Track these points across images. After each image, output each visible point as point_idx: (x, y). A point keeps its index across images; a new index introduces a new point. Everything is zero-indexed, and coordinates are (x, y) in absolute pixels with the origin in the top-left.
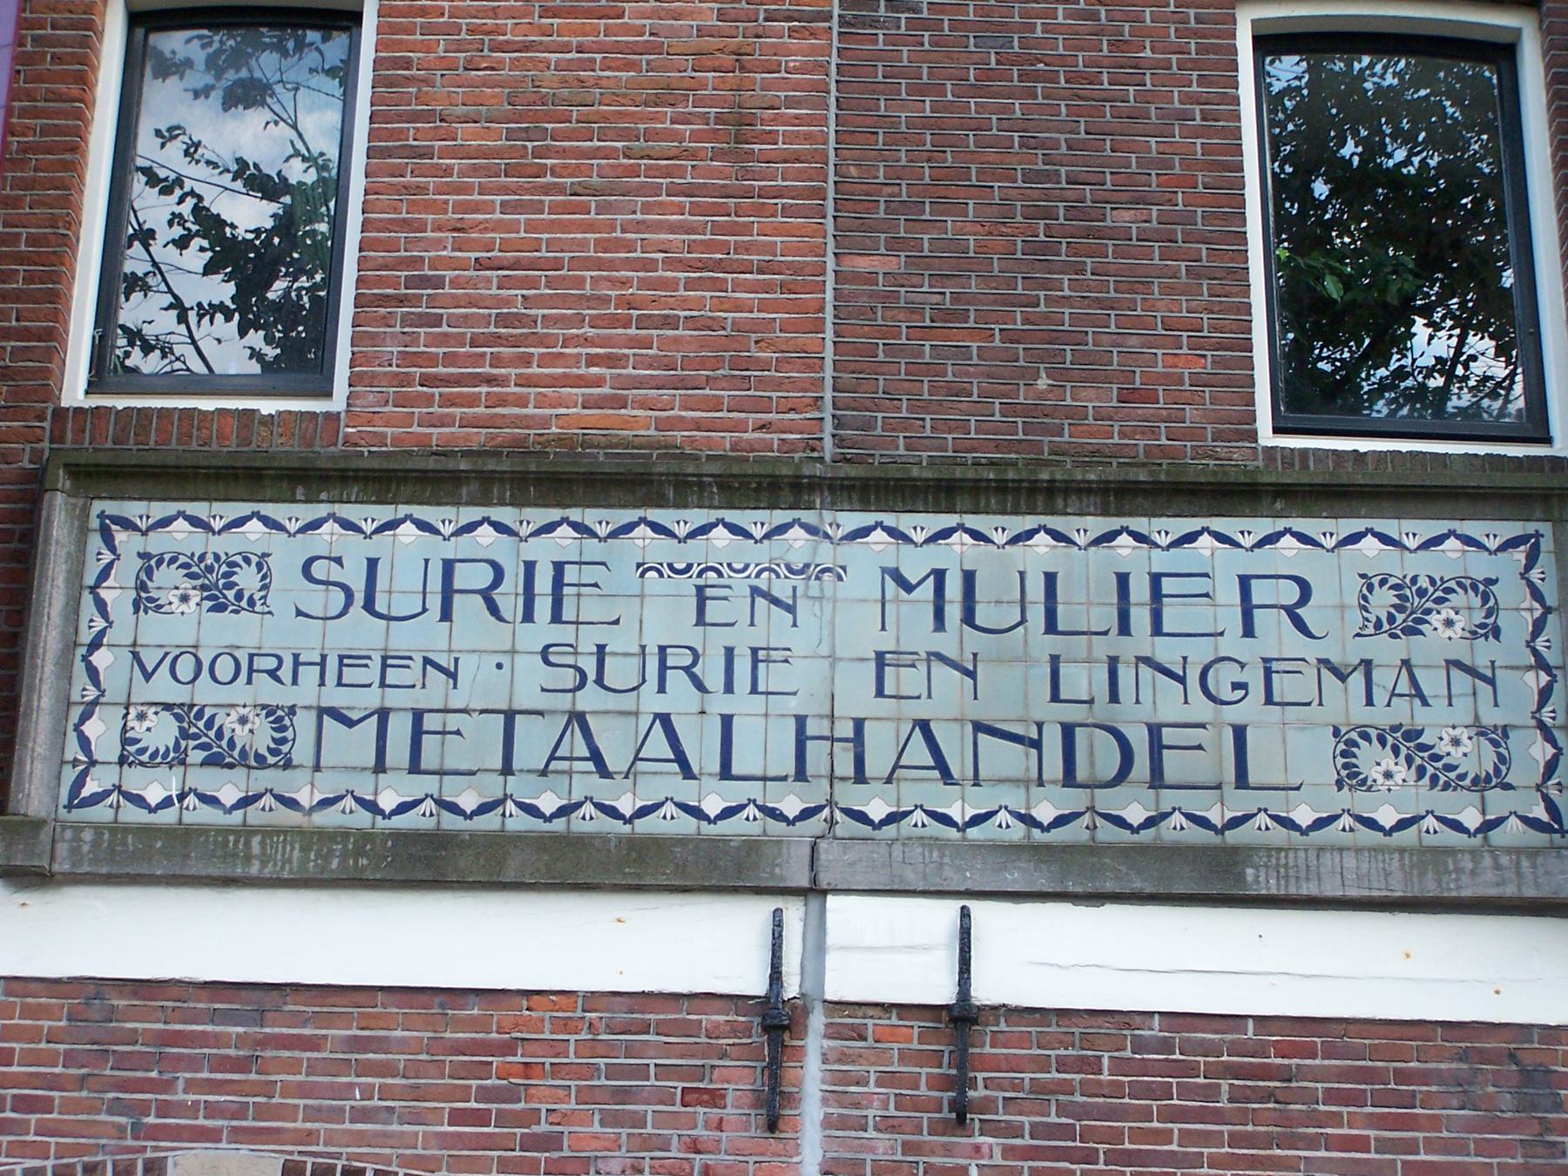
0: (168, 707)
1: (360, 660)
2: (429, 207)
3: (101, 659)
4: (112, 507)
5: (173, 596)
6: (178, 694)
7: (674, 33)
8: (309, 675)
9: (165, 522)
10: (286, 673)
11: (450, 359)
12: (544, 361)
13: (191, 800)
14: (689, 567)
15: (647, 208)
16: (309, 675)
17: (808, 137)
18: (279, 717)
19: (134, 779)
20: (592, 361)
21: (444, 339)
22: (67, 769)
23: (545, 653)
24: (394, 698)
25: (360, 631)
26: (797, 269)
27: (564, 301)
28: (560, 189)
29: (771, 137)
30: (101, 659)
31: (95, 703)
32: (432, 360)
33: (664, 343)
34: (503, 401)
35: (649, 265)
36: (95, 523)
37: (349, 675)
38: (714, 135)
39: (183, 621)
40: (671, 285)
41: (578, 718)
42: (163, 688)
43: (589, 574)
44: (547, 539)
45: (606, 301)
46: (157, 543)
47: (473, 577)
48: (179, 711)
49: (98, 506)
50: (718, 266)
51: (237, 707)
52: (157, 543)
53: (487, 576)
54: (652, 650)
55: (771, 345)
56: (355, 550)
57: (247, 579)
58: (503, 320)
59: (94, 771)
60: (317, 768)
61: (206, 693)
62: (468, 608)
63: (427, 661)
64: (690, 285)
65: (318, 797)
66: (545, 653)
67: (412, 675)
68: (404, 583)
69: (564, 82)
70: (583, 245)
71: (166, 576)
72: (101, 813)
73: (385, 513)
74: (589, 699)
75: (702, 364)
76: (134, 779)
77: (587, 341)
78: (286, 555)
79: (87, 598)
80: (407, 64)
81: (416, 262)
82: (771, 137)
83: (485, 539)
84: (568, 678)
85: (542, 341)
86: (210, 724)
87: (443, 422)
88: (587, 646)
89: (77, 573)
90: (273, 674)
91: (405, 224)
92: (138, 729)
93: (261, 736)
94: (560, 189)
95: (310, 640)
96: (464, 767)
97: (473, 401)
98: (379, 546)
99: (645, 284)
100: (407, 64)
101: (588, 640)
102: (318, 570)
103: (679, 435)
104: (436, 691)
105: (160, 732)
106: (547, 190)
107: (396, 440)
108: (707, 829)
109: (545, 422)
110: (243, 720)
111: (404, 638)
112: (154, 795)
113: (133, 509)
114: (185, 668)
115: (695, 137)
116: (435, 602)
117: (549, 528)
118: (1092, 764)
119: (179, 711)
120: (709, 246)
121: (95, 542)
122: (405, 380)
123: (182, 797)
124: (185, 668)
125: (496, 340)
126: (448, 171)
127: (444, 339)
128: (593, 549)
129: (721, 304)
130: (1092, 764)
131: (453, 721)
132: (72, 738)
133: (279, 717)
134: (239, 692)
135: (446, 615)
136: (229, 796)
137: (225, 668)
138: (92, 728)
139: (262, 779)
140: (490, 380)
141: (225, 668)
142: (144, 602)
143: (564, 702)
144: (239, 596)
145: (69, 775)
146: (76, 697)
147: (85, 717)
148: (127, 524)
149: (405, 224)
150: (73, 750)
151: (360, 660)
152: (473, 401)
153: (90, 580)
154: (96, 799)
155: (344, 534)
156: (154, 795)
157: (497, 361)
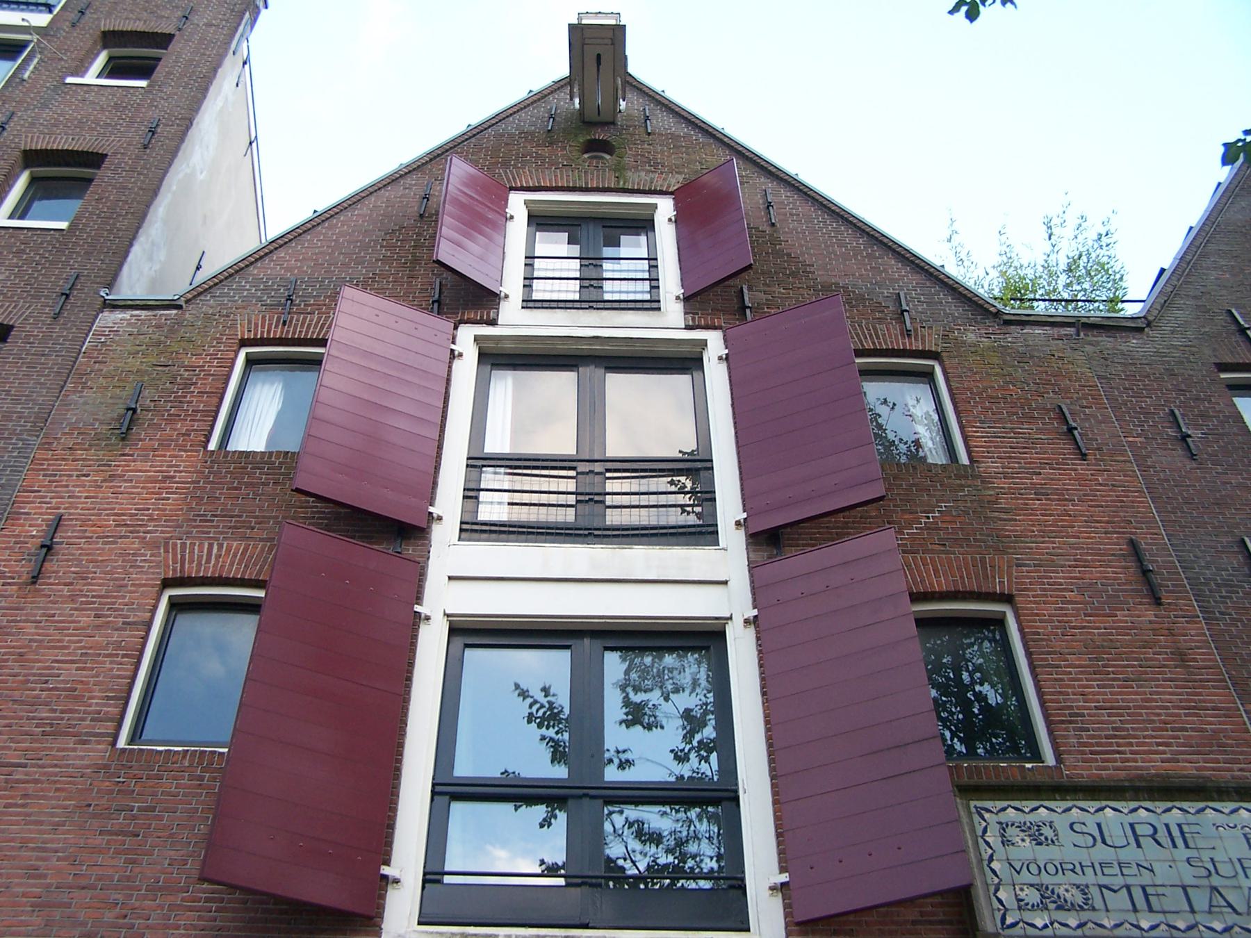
0: (1032, 885)
1: (1109, 865)
2: (1068, 686)
3: (995, 865)
4: (979, 804)
5: (1018, 839)
6: (1035, 880)
7: (1141, 622)
8: (1089, 871)
9: (1004, 809)
10: (1078, 869)
11: (1098, 744)
12: (1138, 744)
13: (1056, 925)
14: (1235, 826)
15: (1157, 686)
16: (1089, 871)
17: (1210, 660)
18: (1083, 889)
19: (1028, 916)
20: (1158, 744)
21: (1093, 737)
22: (996, 913)
23: (1188, 860)
24: (1130, 881)
25: (1101, 853)
26: (1228, 709)
27: (1137, 722)
28: (1119, 680)
29: (1195, 660)
30: (995, 865)
31: (999, 884)
32: (1092, 745)
33: (1185, 737)
34: (1128, 760)
35: (1167, 708)
36: (973, 810)
37: (1106, 871)
38: (1172, 659)
39: (1024, 848)
40: (1178, 715)
41: (1214, 889)
42: (1025, 877)
43: (1195, 828)
44: (1175, 815)
45: (1154, 721)
46: (1003, 817)
47: (1143, 830)
48: (1038, 887)
49: (972, 803)
50: (1194, 708)
51: (1063, 884)
52: (1003, 817)
53: (1151, 831)
54: (1235, 861)
55: (1230, 738)
56: (1091, 821)
57: (1047, 831)
58: (1115, 729)
59: (1008, 913)
60: (1107, 910)
61: (1045, 879)
62: (1147, 842)
63: (1138, 865)
64: (1186, 715)
65: (1112, 923)
66: (1188, 860)
67: (1134, 870)
68: (1116, 833)
69: (1104, 640)
70: (1136, 700)
71: (1010, 831)
72: (1017, 931)
73: (1097, 804)
74: (1216, 880)
75: (1205, 745)
76: (1028, 916)
77: (1153, 737)
78: (1061, 822)
79: (980, 841)
80: (1039, 634)
81: (1071, 708)
82: (1195, 660)
83: (1145, 814)
84: (1204, 873)
85: (1135, 737)
86: (1053, 892)
87: (1105, 769)
88: (1206, 858)
89: (973, 830)
90: (1072, 870)
91: (1060, 693)
92: (1022, 895)
93: (1079, 899)
94: (1119, 680)
95: (1083, 856)
96: (1173, 909)
97: (1115, 760)
98: (1099, 817)
99: (1167, 715)
100: (1039, 634)
101: (1206, 856)
102: (1076, 827)
103: (1207, 773)
104: (1146, 878)
105: (1032, 896)
106: (1114, 679)
107: (1088, 776)
108: (1145, 934)
109: (1147, 768)
110: (1067, 891)
111: (1124, 855)
112: (1039, 923)
113: (988, 804)
114: (1033, 868)
115: (1164, 659)
116: (1132, 840)
117: (1169, 810)
118: (642, 292)
119: (1038, 887)
120: (1187, 701)
121: (976, 818)
122: (1083, 753)
123: (1052, 924)
124: (1033, 868)
125: (1115, 737)
126: (1070, 673)
127: (1093, 737)
128: (1191, 818)
129: (1202, 723)
130: (642, 292)
131: (1160, 890)
132: (994, 899)
133: (1083, 889)
134: (1060, 878)
135: (1139, 846)
136: (1073, 923)
137: (1051, 868)
138: (1002, 894)
139: (1085, 916)
140: (1119, 752)
141: (1051, 868)
142: (1006, 842)
143: (1205, 882)
144: (1046, 839)
145: (998, 916)
146: (989, 881)
147: (997, 890)
148: (988, 811)
149: (1060, 693)
150: (996, 904)
151: (1109, 865)
152: (1115, 760)
153: (980, 833)
154: (1014, 925)
155: (1084, 813)
156: (1039, 923)
157: (1118, 745)
